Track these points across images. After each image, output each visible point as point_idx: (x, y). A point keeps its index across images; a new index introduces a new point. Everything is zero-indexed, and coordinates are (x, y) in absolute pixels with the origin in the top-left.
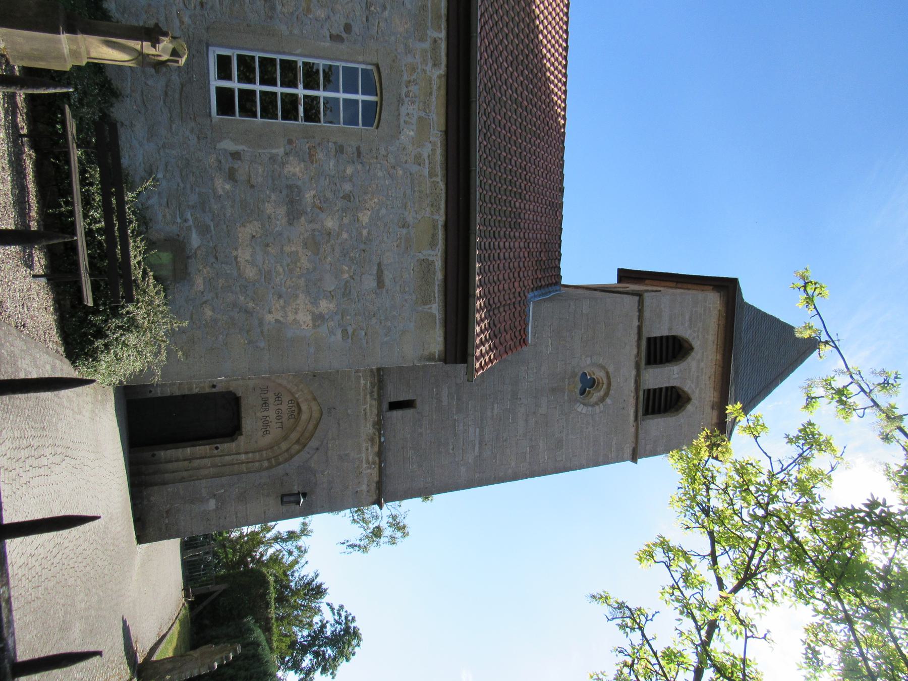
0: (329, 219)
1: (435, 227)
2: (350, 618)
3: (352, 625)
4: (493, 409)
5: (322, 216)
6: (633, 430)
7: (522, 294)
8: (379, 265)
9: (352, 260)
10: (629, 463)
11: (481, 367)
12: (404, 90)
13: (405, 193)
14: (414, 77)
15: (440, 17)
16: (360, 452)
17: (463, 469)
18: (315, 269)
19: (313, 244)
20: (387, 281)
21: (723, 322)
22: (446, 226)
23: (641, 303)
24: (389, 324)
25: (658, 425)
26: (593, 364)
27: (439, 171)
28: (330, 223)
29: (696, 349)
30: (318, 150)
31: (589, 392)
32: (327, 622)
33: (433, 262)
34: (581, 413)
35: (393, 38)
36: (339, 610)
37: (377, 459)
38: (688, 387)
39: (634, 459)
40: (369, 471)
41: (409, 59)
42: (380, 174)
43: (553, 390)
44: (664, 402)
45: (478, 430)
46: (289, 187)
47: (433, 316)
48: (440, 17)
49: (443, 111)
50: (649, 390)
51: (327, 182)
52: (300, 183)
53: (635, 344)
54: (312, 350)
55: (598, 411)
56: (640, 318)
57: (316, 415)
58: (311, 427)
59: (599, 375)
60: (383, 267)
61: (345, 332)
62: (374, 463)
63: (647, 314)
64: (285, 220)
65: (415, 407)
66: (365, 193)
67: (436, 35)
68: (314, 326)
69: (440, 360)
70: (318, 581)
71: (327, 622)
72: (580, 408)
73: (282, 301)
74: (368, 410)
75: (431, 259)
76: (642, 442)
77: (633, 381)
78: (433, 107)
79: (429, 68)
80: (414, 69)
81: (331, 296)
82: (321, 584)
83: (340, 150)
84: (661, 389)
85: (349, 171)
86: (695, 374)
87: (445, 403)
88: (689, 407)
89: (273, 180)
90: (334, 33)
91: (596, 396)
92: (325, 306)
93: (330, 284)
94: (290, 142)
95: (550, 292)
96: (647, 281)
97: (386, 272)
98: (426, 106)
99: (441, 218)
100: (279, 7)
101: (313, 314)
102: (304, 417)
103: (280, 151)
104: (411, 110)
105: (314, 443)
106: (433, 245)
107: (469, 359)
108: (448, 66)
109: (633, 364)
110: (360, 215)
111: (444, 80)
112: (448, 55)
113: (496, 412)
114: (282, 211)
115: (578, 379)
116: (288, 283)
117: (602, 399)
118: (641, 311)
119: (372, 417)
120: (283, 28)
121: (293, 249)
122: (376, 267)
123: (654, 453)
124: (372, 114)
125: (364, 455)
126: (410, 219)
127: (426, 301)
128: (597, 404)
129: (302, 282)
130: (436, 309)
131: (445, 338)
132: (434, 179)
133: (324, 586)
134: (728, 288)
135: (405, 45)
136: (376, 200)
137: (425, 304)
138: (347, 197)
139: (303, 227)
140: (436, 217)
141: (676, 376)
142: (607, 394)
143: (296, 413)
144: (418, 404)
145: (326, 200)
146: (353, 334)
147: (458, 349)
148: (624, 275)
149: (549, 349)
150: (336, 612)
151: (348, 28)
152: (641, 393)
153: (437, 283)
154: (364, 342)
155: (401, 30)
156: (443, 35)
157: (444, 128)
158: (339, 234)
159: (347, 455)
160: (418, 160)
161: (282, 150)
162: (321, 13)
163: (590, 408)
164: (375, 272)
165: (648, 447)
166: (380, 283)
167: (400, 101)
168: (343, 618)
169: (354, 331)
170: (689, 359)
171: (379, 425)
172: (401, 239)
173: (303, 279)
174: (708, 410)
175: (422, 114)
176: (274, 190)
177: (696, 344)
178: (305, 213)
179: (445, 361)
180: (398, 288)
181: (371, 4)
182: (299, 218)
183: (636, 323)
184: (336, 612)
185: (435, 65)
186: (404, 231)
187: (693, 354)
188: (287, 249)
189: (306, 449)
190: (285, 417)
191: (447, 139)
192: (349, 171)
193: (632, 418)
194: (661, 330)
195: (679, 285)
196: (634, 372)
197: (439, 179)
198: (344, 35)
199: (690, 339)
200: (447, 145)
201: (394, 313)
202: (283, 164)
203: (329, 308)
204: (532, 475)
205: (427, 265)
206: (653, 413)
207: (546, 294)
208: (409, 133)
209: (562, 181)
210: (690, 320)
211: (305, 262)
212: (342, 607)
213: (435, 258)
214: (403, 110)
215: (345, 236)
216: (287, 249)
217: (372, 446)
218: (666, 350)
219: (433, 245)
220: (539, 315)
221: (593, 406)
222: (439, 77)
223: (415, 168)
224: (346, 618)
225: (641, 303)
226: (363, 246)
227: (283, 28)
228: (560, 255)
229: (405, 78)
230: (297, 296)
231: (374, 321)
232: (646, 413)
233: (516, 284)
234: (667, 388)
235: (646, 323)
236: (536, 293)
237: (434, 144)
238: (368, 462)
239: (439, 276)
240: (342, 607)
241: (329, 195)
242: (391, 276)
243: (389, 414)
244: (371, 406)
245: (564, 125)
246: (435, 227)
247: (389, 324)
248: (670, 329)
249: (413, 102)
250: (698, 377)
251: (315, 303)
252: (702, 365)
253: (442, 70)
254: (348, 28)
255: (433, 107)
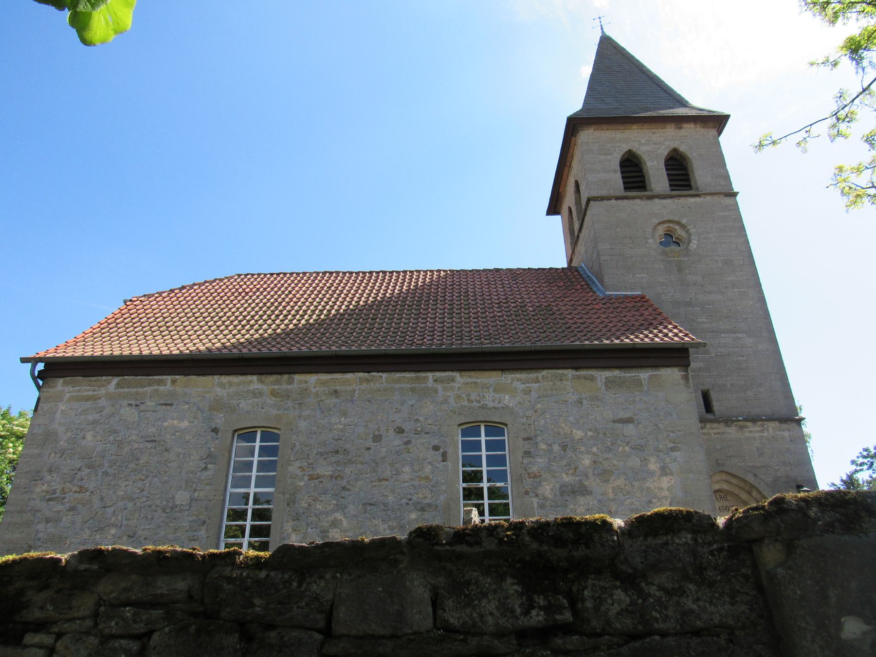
0: (583, 462)
1: (578, 377)
2: (865, 453)
3: (873, 451)
4: (702, 323)
5: (581, 467)
6: (708, 198)
7: (603, 302)
8: (614, 422)
9: (613, 444)
10: (738, 198)
11: (686, 335)
12: (475, 404)
13: (556, 402)
14: (464, 396)
15: (417, 378)
16: (754, 438)
17: (760, 347)
18: (625, 474)
19: (605, 475)
20: (626, 415)
21: (605, 126)
22: (576, 368)
23: (595, 199)
24: (662, 413)
25: (700, 175)
26: (653, 237)
27: (533, 375)
28: (587, 461)
29: (630, 148)
30: (530, 471)
31: (676, 238)
32: (871, 477)
33: (606, 378)
34: (698, 245)
35: (438, 413)
36: (857, 465)
37: (759, 423)
38: (664, 152)
39: (734, 195)
40: (770, 430)
41: (452, 400)
42: (542, 422)
43: (680, 270)
44: (679, 170)
45: (723, 335)
46: (562, 493)
47: (651, 377)
48: (417, 378)
49: (487, 373)
50: (671, 185)
51: (555, 464)
52: (558, 486)
53: (631, 201)
54: (691, 476)
55: (695, 230)
56: (608, 198)
57: (724, 476)
58: (734, 481)
59: (661, 230)
60: (616, 418)
61: (672, 449)
62: (763, 425)
63: (604, 193)
64: (588, 497)
65: (708, 390)
66: (559, 433)
67: (431, 380)
68: (672, 474)
69: (687, 371)
70: (845, 478)
71: (871, 477)
72: (693, 245)
73: (654, 500)
74: (716, 431)
75: (604, 380)
76: (719, 189)
77: (664, 201)
78: (485, 381)
79: (457, 385)
80: (459, 397)
81: (645, 461)
82: (842, 480)
83: (527, 454)
84: (668, 175)
85: (544, 447)
86: (653, 146)
87: (702, 365)
88: (682, 149)
89: (558, 506)
90: (441, 459)
91: (680, 232)
92: (653, 466)
93: (635, 461)
94: (527, 493)
95: (588, 276)
96: (561, 190)
97: (620, 416)
98: (485, 387)
99: (570, 373)
100: (428, 501)
101: (661, 475)
102: (725, 487)
103: (535, 500)
104: (490, 397)
105: (750, 478)
106: (592, 379)
107: (686, 346)
108: (453, 371)
109: (649, 202)
110: (577, 437)
111: (463, 373)
112: (444, 371)
113: (704, 320)
114: (581, 500)
115: (667, 249)
116: (638, 495)
117: (683, 227)
118: (602, 199)
119: (722, 428)
120: (442, 498)
121: (610, 491)
122: (617, 424)
123: (727, 177)
124: (494, 429)
125: (757, 435)
126: (575, 398)
127: (639, 383)
128: (687, 231)
129: (636, 484)
130: (644, 375)
131: (668, 366)
132: (540, 378)
133: (845, 478)
134: (574, 125)
135: (442, 403)
136: (563, 425)
137: (641, 384)
138: (564, 448)
139: (592, 483)
140: (570, 376)
141: (655, 163)
142: (678, 223)
143: (722, 494)
144: (705, 388)
145: (569, 464)
146: (674, 442)
147: (676, 356)
148: (553, 209)
149: (643, 275)
150: (858, 468)
151: (436, 448)
152: (674, 193)
153: (623, 375)
154: (679, 433)
155: (431, 407)
156: (430, 375)
157: (499, 373)
158: (594, 454)
159: (758, 449)
160: (527, 392)
161: (533, 499)
162: (428, 469)
163: (693, 237)
164: (621, 425)
165: (723, 183)
166: (629, 421)
167: (484, 407)
168: (865, 461)
169: (671, 441)
170: (639, 152)
171: (728, 421)
172: (591, 405)
173: (635, 483)
174: (683, 132)
175: (491, 390)
176: (566, 506)
177: (625, 148)
178: (581, 481)
179: (687, 365)
180: (631, 406)
181: (416, 430)
182: (585, 487)
183: (613, 202)
184: (858, 468)
185: (453, 380)
186: (585, 402)
187: (634, 150)
188: (611, 496)
189: (756, 485)
190: (726, 503)
191: (509, 369)
192: (544, 447)
193: (697, 199)
194: (617, 179)
195: (568, 164)
196: (656, 201)
197: (540, 375)
198: (441, 451)
199: (622, 153)
200: (513, 369)
201: (652, 409)
202: (545, 499)
203: (655, 463)
204: (758, 285)
205: (609, 383)
206: (688, 180)
207: (591, 280)
208: (507, 399)
209: (490, 270)
210: (605, 154)
211: (620, 482)
212: (853, 462)
213: (603, 377)
214: (491, 404)
215: (595, 449)
216: (611, 496)
217: (746, 427)
218: (632, 171)
219: (592, 379)
220: (619, 284)
221: (690, 235)
222: (462, 377)
223: (534, 394)
224: (864, 457)
225: (595, 199)
226: (601, 435)
227: (442, 498)
228: (551, 269)
229: (466, 403)
230: (648, 488)
231: (660, 425)
232: (688, 186)
233: (597, 307)
234: (667, 170)
235: (612, 193)
236: (595, 289)
237: (513, 380)
238: (762, 431)
239: (617, 373)
240: (853, 462)
241: (564, 462)
242: (622, 413)
243: (717, 413)
244: (711, 428)
245: (444, 271)
246: (578, 377)
247: (662, 413)
248: (615, 171)
249: (484, 397)
250: (654, 144)
251: (652, 474)
252: (643, 141)
253: (456, 374)
254: (436, 448)
255: (485, 381)
